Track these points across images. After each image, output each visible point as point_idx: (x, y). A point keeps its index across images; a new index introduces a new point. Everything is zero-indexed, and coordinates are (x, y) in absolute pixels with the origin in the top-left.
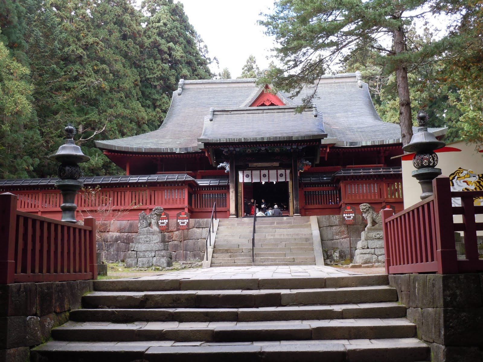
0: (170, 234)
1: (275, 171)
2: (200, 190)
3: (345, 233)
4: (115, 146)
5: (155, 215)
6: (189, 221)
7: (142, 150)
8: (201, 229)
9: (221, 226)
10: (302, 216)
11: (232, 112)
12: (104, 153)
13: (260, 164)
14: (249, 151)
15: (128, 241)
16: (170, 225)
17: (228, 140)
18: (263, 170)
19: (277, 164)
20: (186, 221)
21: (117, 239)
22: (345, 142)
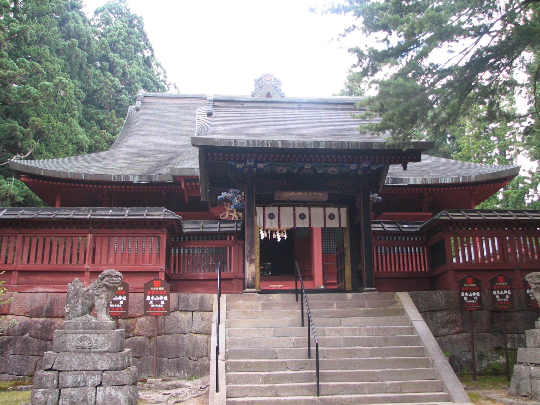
0: (130, 322)
3: (458, 324)
4: (40, 169)
5: (104, 289)
6: (169, 298)
7: (82, 177)
8: (190, 314)
9: (232, 308)
11: (246, 105)
12: (22, 179)
13: (300, 195)
14: (281, 170)
15: (45, 338)
16: (130, 304)
17: (251, 143)
18: (299, 206)
19: (322, 196)
20: (163, 299)
21: (24, 330)
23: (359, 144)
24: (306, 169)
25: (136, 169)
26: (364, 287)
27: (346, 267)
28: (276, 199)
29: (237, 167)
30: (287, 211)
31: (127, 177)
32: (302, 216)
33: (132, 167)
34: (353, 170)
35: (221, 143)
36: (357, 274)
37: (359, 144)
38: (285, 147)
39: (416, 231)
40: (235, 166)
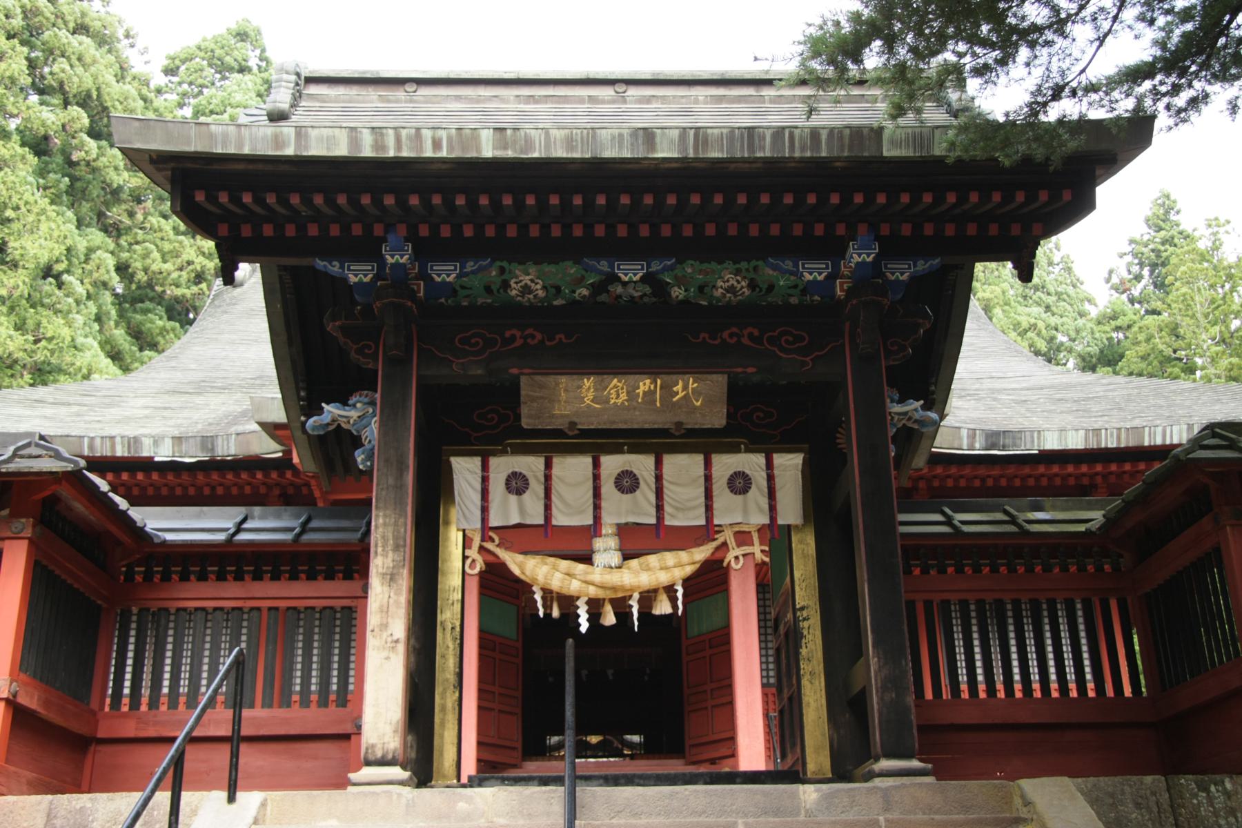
1: (694, 462)
2: (148, 577)
10: (941, 772)
14: (526, 290)
18: (617, 450)
19: (695, 394)
22: (964, 433)
23: (824, 135)
24: (625, 284)
25: (172, 422)
26: (877, 760)
27: (805, 682)
28: (525, 423)
29: (353, 279)
30: (573, 470)
31: (135, 441)
32: (626, 482)
33: (164, 418)
34: (815, 281)
35: (240, 143)
36: (847, 706)
37: (824, 135)
38: (510, 154)
39: (1088, 533)
40: (345, 280)
